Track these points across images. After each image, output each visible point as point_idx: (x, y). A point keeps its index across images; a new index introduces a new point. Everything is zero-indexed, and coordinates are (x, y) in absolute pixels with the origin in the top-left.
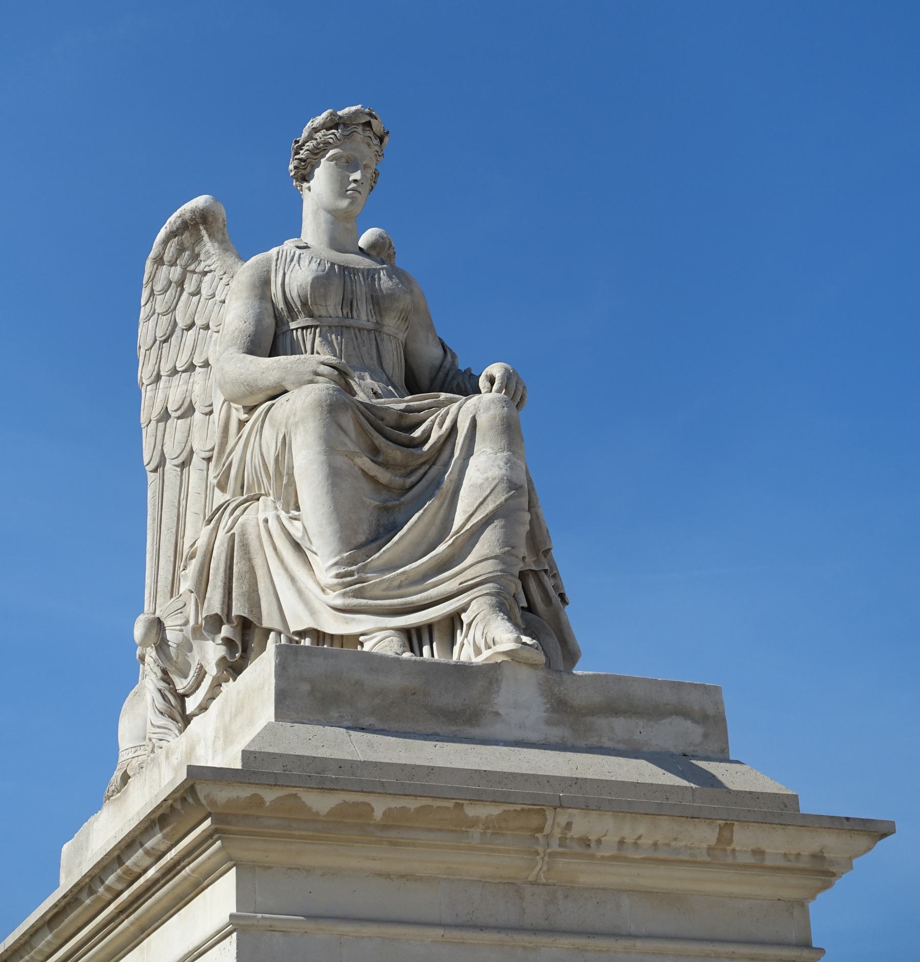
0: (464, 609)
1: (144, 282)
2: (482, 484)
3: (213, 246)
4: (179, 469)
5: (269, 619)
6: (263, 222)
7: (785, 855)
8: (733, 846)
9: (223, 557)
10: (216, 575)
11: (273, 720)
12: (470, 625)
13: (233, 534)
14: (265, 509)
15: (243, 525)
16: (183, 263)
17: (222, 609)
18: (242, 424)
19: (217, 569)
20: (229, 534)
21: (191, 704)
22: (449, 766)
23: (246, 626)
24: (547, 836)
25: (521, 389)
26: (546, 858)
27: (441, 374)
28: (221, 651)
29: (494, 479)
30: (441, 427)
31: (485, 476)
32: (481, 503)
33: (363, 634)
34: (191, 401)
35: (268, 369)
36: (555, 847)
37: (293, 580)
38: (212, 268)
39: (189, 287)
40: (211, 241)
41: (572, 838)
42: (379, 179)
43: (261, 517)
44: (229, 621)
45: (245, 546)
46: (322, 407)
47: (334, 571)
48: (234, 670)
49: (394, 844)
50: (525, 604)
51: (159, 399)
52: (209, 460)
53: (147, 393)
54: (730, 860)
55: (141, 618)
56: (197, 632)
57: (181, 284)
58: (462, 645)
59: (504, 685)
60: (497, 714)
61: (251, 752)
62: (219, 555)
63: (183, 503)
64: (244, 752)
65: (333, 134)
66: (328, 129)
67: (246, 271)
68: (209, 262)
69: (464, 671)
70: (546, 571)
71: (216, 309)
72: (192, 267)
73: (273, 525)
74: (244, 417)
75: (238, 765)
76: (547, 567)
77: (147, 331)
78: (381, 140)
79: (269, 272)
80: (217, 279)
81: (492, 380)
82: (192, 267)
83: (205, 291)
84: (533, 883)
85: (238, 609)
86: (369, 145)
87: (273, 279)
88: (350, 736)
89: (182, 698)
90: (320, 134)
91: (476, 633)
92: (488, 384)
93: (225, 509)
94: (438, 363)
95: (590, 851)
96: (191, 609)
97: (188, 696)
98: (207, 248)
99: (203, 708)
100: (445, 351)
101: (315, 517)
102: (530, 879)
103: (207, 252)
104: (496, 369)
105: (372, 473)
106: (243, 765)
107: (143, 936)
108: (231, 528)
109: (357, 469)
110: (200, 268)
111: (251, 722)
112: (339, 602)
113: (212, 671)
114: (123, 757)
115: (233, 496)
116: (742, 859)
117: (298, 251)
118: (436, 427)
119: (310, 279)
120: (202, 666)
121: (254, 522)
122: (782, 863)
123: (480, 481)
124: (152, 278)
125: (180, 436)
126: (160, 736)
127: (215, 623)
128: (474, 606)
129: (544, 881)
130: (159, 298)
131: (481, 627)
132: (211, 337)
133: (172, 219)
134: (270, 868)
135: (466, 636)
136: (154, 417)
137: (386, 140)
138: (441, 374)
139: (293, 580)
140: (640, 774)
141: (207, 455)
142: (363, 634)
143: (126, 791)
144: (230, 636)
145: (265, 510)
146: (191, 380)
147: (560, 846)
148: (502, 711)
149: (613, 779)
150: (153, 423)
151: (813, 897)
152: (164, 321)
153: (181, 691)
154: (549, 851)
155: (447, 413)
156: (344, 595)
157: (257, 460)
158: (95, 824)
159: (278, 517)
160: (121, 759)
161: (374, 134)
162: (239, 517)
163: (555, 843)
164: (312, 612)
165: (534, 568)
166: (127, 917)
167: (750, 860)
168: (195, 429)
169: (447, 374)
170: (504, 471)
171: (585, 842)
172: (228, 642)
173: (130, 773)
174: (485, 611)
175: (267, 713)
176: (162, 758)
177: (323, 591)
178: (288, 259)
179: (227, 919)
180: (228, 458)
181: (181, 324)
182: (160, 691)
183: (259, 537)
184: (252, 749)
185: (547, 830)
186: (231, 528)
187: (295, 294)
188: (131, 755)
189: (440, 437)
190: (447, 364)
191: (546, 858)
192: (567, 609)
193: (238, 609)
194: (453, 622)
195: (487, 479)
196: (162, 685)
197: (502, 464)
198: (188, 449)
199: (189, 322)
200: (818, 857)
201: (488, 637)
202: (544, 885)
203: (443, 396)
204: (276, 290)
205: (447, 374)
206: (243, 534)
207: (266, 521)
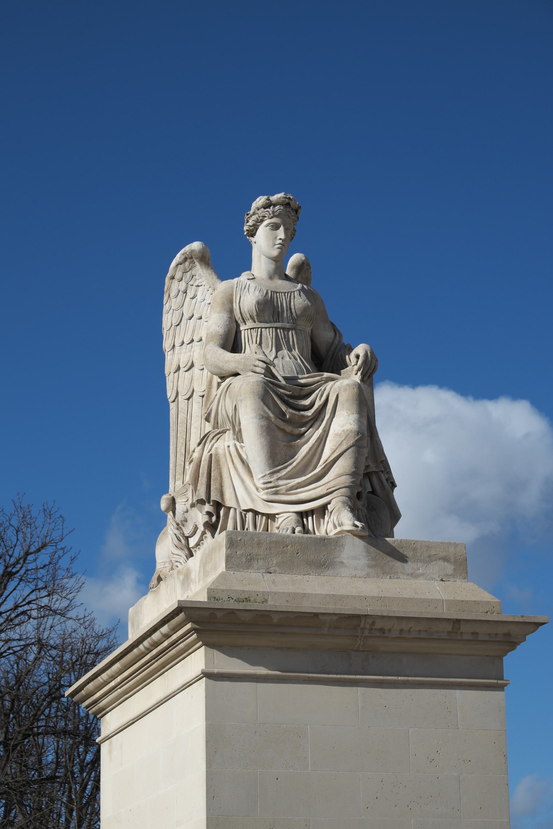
0: (329, 503)
1: (165, 290)
2: (341, 433)
3: (203, 272)
4: (187, 401)
5: (229, 501)
6: (229, 260)
7: (489, 634)
8: (461, 631)
9: (206, 468)
10: (202, 476)
11: (224, 570)
12: (331, 512)
13: (211, 455)
14: (228, 439)
15: (216, 448)
16: (187, 280)
17: (206, 496)
18: (219, 385)
19: (203, 474)
20: (209, 454)
21: (192, 542)
22: (314, 592)
23: (218, 505)
24: (363, 629)
25: (374, 362)
26: (362, 639)
27: (333, 348)
28: (206, 518)
29: (347, 431)
30: (320, 399)
31: (342, 429)
32: (340, 445)
33: (278, 514)
34: (193, 362)
35: (230, 360)
36: (366, 633)
37: (243, 481)
38: (203, 284)
39: (190, 294)
40: (202, 268)
41: (375, 629)
42: (296, 233)
43: (226, 444)
44: (209, 503)
45: (218, 461)
46: (254, 392)
47: (262, 481)
48: (213, 527)
49: (283, 634)
50: (370, 490)
51: (175, 361)
52: (203, 396)
53: (169, 357)
54: (459, 638)
55: (165, 497)
56: (193, 506)
57: (185, 292)
58: (328, 522)
59: (346, 547)
60: (342, 563)
61: (212, 589)
62: (205, 460)
63: (189, 421)
64: (208, 589)
65: (267, 211)
66: (265, 208)
67: (223, 286)
68: (200, 280)
69: (325, 541)
70: (382, 471)
71: (206, 308)
72: (191, 283)
73: (232, 449)
74: (219, 380)
75: (206, 600)
76: (383, 469)
77: (168, 319)
78: (296, 211)
79: (232, 295)
80: (206, 290)
81: (358, 357)
82: (191, 283)
83: (199, 297)
84: (357, 651)
85: (214, 496)
86: (289, 216)
87: (234, 300)
88: (264, 577)
89: (187, 538)
90: (260, 211)
91: (334, 517)
92: (355, 360)
93: (208, 437)
94: (331, 341)
95: (385, 635)
96: (190, 493)
97: (190, 537)
98: (200, 272)
99: (198, 545)
100: (336, 334)
101: (253, 446)
102: (354, 649)
103: (200, 274)
104: (360, 349)
105: (282, 427)
106: (209, 598)
107: (163, 670)
108: (210, 451)
109: (274, 425)
110: (196, 284)
111: (215, 568)
112: (265, 497)
113: (201, 528)
114: (159, 567)
115: (214, 429)
116: (465, 637)
117: (249, 282)
118: (318, 399)
119: (254, 302)
120: (196, 525)
121: (222, 448)
122: (487, 638)
123: (340, 432)
124: (169, 288)
125: (187, 382)
126: (177, 559)
127: (201, 502)
128: (333, 502)
129: (362, 649)
130: (174, 300)
131: (336, 514)
132: (203, 325)
133: (178, 255)
134: (222, 646)
135: (330, 518)
136: (173, 370)
137: (299, 211)
138: (333, 348)
139: (243, 481)
140: (416, 593)
141: (202, 394)
142: (278, 514)
143: (159, 588)
144: (209, 510)
145: (228, 441)
146: (193, 350)
147: (369, 633)
148: (345, 561)
149: (401, 596)
150: (172, 374)
151: (506, 655)
152: (177, 314)
153: (187, 535)
154: (364, 635)
155: (325, 389)
156: (267, 493)
157: (224, 412)
158: (145, 601)
159: (235, 445)
160: (157, 568)
161: (292, 209)
162: (214, 444)
163: (366, 633)
164: (252, 500)
165: (375, 470)
166: (156, 661)
167: (470, 637)
168: (195, 378)
169: (336, 348)
170: (353, 426)
171: (382, 630)
172: (209, 514)
173: (162, 577)
174: (339, 506)
175: (222, 567)
176: (175, 575)
177: (257, 489)
178: (243, 288)
179: (200, 672)
180: (210, 405)
181: (186, 316)
182: (175, 535)
183: (225, 455)
184: (213, 587)
185: (362, 625)
186: (210, 451)
187: (246, 310)
188: (162, 566)
189: (319, 406)
190: (336, 342)
191: (362, 639)
192: (396, 491)
193: (214, 496)
194: (323, 509)
195: (344, 431)
196: (177, 532)
197: (352, 422)
198: (191, 390)
199: (190, 315)
200: (508, 635)
201: (340, 521)
202: (362, 651)
203: (326, 375)
204: (236, 307)
205: (336, 348)
206: (217, 454)
207: (229, 446)
